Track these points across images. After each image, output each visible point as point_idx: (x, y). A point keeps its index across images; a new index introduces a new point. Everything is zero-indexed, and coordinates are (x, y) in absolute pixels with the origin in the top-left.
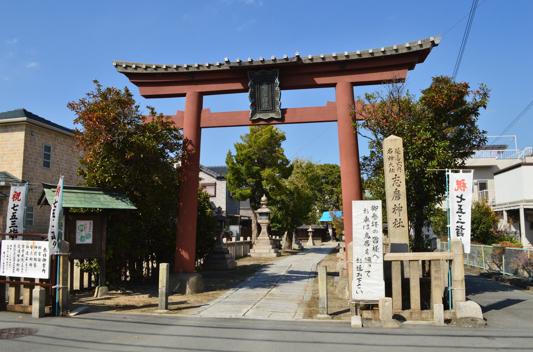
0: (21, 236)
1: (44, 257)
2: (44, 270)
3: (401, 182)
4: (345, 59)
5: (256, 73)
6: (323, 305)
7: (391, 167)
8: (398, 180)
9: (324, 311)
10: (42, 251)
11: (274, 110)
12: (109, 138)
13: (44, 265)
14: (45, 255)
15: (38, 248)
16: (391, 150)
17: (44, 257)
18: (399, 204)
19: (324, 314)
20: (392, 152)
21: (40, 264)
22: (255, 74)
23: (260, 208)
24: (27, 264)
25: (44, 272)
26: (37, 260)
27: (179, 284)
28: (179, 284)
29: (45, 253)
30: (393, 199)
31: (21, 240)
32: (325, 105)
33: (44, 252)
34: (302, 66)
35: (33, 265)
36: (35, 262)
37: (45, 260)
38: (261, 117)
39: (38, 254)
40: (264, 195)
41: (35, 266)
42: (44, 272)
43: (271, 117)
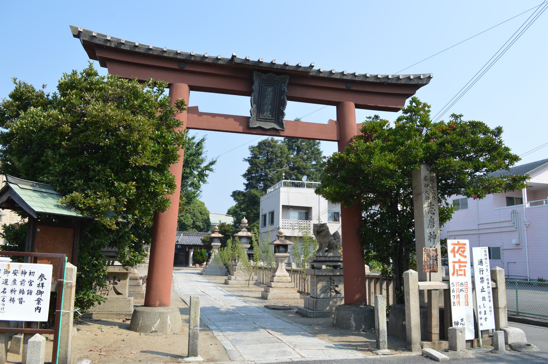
0: (472, 249)
1: (40, 289)
2: (38, 309)
3: (435, 210)
4: (349, 79)
5: (263, 76)
6: (384, 339)
7: (427, 195)
8: (433, 208)
9: (384, 345)
10: (36, 279)
11: (259, 119)
12: (14, 128)
13: (39, 301)
14: (40, 285)
15: (28, 274)
16: (427, 178)
17: (40, 289)
18: (434, 232)
19: (384, 349)
20: (427, 179)
21: (30, 301)
22: (262, 77)
23: (240, 231)
24: (4, 299)
25: (38, 310)
26: (26, 292)
27: (159, 321)
28: (159, 321)
29: (42, 282)
30: (428, 227)
31: (31, 263)
32: (326, 123)
33: (40, 280)
34: (310, 77)
35: (17, 301)
36: (21, 296)
37: (41, 293)
38: (261, 126)
39: (27, 284)
40: (28, 217)
41: (21, 303)
42: (38, 310)
43: (272, 127)
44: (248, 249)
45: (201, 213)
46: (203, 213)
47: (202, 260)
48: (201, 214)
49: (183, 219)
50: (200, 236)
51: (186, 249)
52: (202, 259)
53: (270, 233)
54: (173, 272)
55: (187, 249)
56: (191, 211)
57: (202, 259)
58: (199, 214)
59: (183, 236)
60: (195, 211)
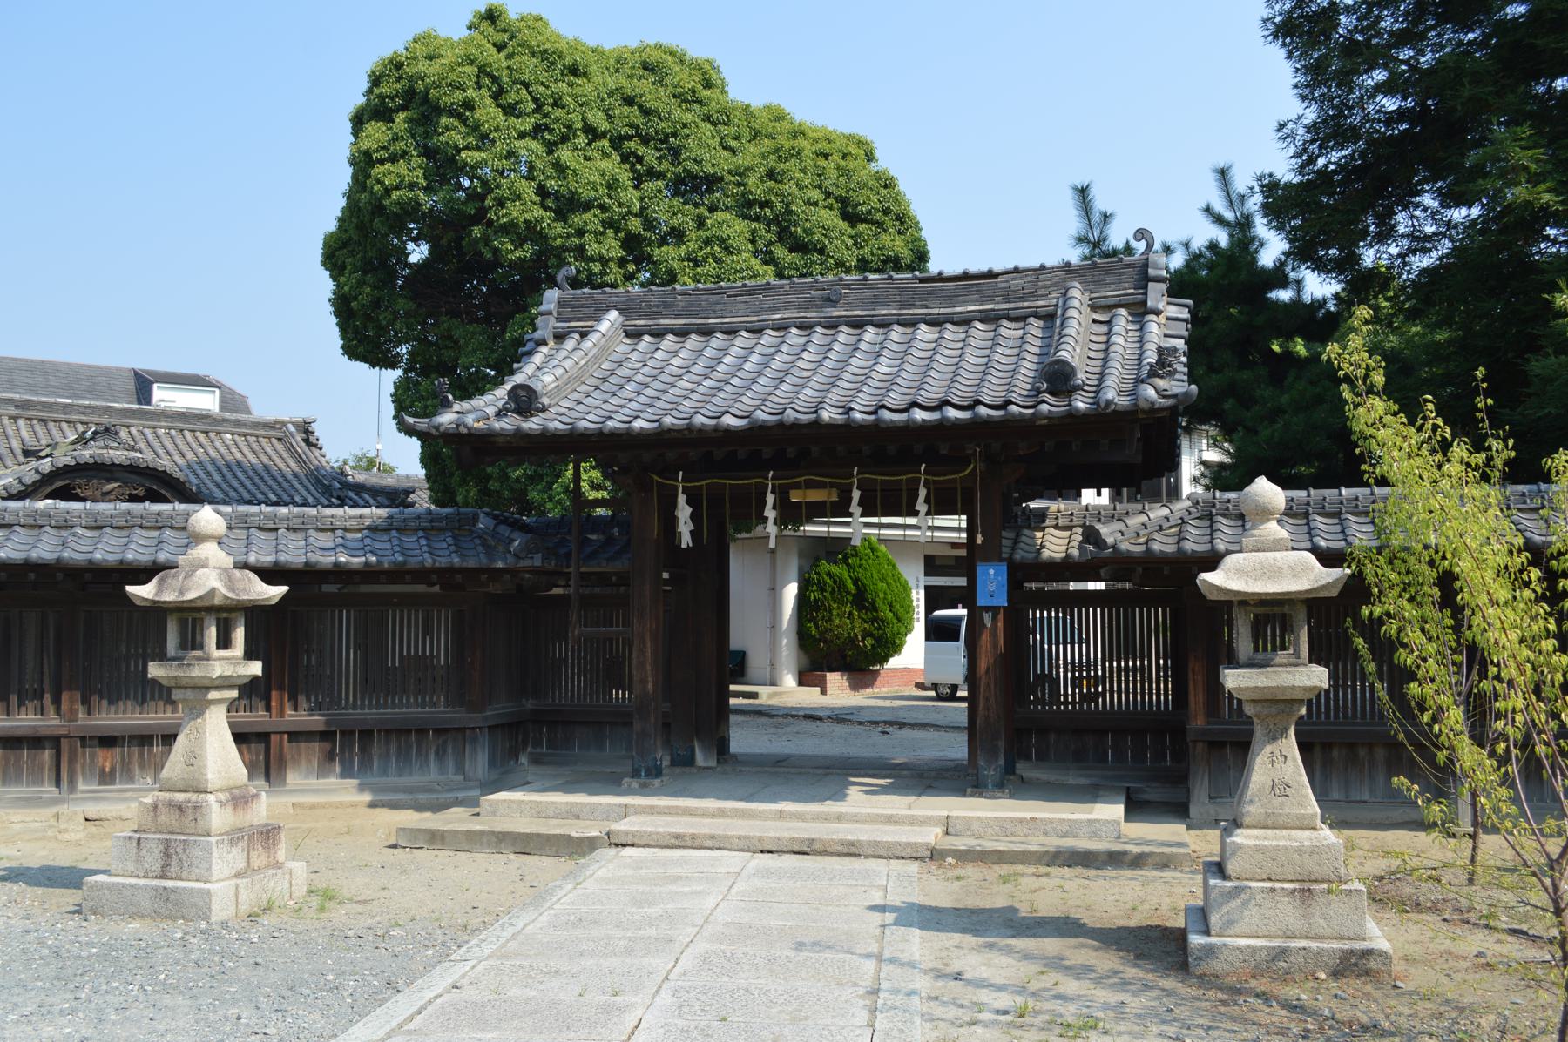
44: (242, 689)
45: (851, 216)
46: (869, 201)
47: (869, 642)
48: (845, 216)
49: (676, 265)
50: (858, 325)
51: (672, 521)
52: (866, 634)
53: (468, 732)
54: (964, 535)
55: (684, 512)
56: (756, 186)
57: (866, 634)
58: (829, 217)
59: (624, 345)
60: (791, 187)
